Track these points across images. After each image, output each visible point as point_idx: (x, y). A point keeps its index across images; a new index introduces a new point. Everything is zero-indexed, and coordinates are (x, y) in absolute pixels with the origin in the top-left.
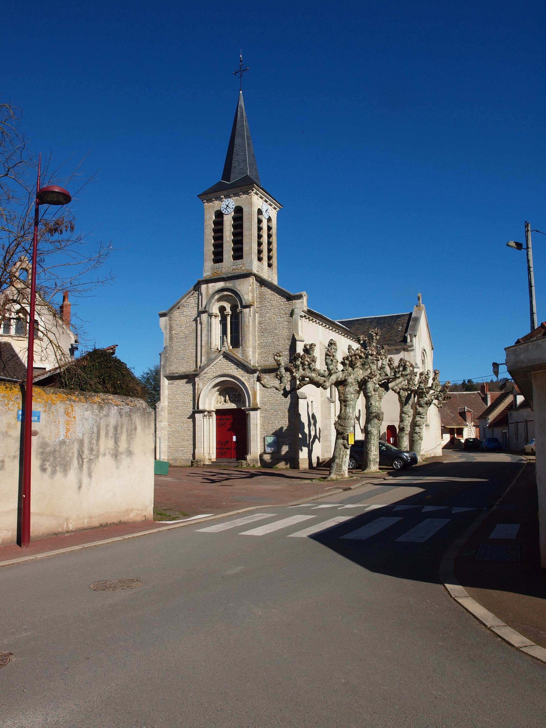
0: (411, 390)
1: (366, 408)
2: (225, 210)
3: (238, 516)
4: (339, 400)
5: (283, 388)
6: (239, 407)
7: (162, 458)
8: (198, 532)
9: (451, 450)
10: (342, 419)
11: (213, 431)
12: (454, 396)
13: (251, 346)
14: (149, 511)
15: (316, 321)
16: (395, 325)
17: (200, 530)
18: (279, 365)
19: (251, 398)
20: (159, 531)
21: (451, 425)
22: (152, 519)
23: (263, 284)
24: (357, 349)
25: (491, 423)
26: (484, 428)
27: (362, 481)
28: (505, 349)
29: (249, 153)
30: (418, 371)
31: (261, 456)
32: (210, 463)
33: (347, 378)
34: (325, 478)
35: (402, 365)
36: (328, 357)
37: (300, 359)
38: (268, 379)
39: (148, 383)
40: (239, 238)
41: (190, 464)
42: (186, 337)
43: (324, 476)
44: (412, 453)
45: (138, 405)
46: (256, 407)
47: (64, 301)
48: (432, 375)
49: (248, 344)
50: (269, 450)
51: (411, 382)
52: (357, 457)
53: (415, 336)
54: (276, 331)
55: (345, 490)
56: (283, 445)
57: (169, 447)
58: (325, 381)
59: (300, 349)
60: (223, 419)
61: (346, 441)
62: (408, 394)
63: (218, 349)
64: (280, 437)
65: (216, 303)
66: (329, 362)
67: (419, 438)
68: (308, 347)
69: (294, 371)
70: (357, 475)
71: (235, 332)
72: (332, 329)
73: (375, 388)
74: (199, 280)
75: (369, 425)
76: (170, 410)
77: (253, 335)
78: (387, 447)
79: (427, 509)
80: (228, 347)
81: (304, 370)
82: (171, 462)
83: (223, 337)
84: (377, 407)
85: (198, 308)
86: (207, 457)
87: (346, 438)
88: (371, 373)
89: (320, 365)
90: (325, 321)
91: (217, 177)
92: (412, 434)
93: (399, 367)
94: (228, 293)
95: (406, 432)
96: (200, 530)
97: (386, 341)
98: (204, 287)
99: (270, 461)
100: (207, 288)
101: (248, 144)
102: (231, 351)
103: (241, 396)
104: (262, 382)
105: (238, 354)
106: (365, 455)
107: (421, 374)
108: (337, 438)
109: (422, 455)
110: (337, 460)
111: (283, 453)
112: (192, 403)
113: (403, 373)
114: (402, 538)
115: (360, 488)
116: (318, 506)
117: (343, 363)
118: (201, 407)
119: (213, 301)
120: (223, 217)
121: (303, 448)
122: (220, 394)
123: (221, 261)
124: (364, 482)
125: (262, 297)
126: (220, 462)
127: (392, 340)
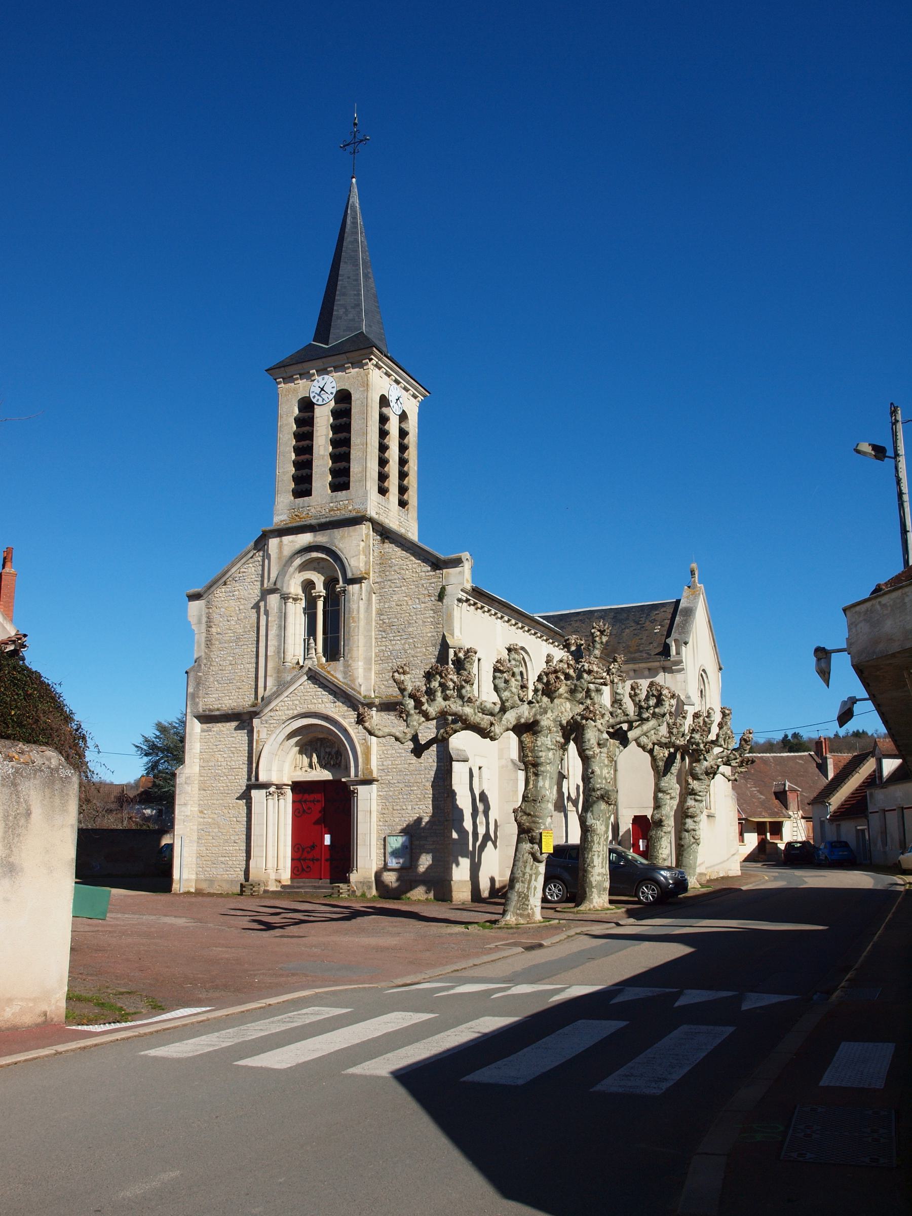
0: (674, 745)
2: (317, 397)
3: (268, 1012)
5: (409, 736)
6: (337, 778)
7: (185, 876)
8: (146, 1056)
9: (759, 865)
11: (285, 824)
12: (764, 761)
13: (361, 657)
14: (56, 1003)
15: (489, 611)
16: (648, 623)
17: (153, 1052)
19: (360, 760)
20: (58, 1053)
21: (760, 815)
22: (63, 1019)
23: (387, 538)
24: (561, 661)
25: (835, 812)
27: (570, 928)
28: (845, 610)
29: (366, 291)
31: (378, 875)
32: (279, 889)
33: (538, 717)
34: (494, 922)
35: (653, 695)
36: (498, 674)
38: (376, 718)
41: (237, 889)
45: (39, 761)
46: (369, 777)
47: (3, 568)
48: (717, 718)
50: (393, 863)
51: (675, 731)
52: (566, 876)
53: (686, 643)
54: (410, 629)
55: (530, 948)
57: (200, 856)
58: (492, 724)
60: (305, 801)
61: (536, 847)
62: (670, 754)
63: (298, 663)
65: (297, 575)
66: (502, 685)
67: (693, 840)
68: (461, 655)
69: (424, 700)
71: (332, 634)
73: (599, 740)
74: (264, 529)
75: (589, 814)
76: (204, 782)
77: (365, 637)
79: (691, 997)
81: (446, 698)
82: (204, 886)
84: (606, 778)
85: (262, 584)
89: (486, 694)
90: (508, 611)
91: (306, 337)
93: (647, 698)
95: (665, 829)
96: (153, 1052)
97: (631, 653)
98: (273, 543)
99: (395, 885)
100: (280, 546)
101: (366, 276)
102: (323, 668)
104: (367, 724)
105: (336, 673)
106: (581, 874)
107: (696, 716)
109: (701, 874)
110: (518, 886)
111: (422, 869)
112: (246, 770)
113: (657, 710)
114: (611, 1084)
115: (563, 944)
116: (453, 987)
118: (263, 778)
119: (291, 569)
122: (301, 752)
125: (384, 563)
126: (298, 887)
127: (641, 652)
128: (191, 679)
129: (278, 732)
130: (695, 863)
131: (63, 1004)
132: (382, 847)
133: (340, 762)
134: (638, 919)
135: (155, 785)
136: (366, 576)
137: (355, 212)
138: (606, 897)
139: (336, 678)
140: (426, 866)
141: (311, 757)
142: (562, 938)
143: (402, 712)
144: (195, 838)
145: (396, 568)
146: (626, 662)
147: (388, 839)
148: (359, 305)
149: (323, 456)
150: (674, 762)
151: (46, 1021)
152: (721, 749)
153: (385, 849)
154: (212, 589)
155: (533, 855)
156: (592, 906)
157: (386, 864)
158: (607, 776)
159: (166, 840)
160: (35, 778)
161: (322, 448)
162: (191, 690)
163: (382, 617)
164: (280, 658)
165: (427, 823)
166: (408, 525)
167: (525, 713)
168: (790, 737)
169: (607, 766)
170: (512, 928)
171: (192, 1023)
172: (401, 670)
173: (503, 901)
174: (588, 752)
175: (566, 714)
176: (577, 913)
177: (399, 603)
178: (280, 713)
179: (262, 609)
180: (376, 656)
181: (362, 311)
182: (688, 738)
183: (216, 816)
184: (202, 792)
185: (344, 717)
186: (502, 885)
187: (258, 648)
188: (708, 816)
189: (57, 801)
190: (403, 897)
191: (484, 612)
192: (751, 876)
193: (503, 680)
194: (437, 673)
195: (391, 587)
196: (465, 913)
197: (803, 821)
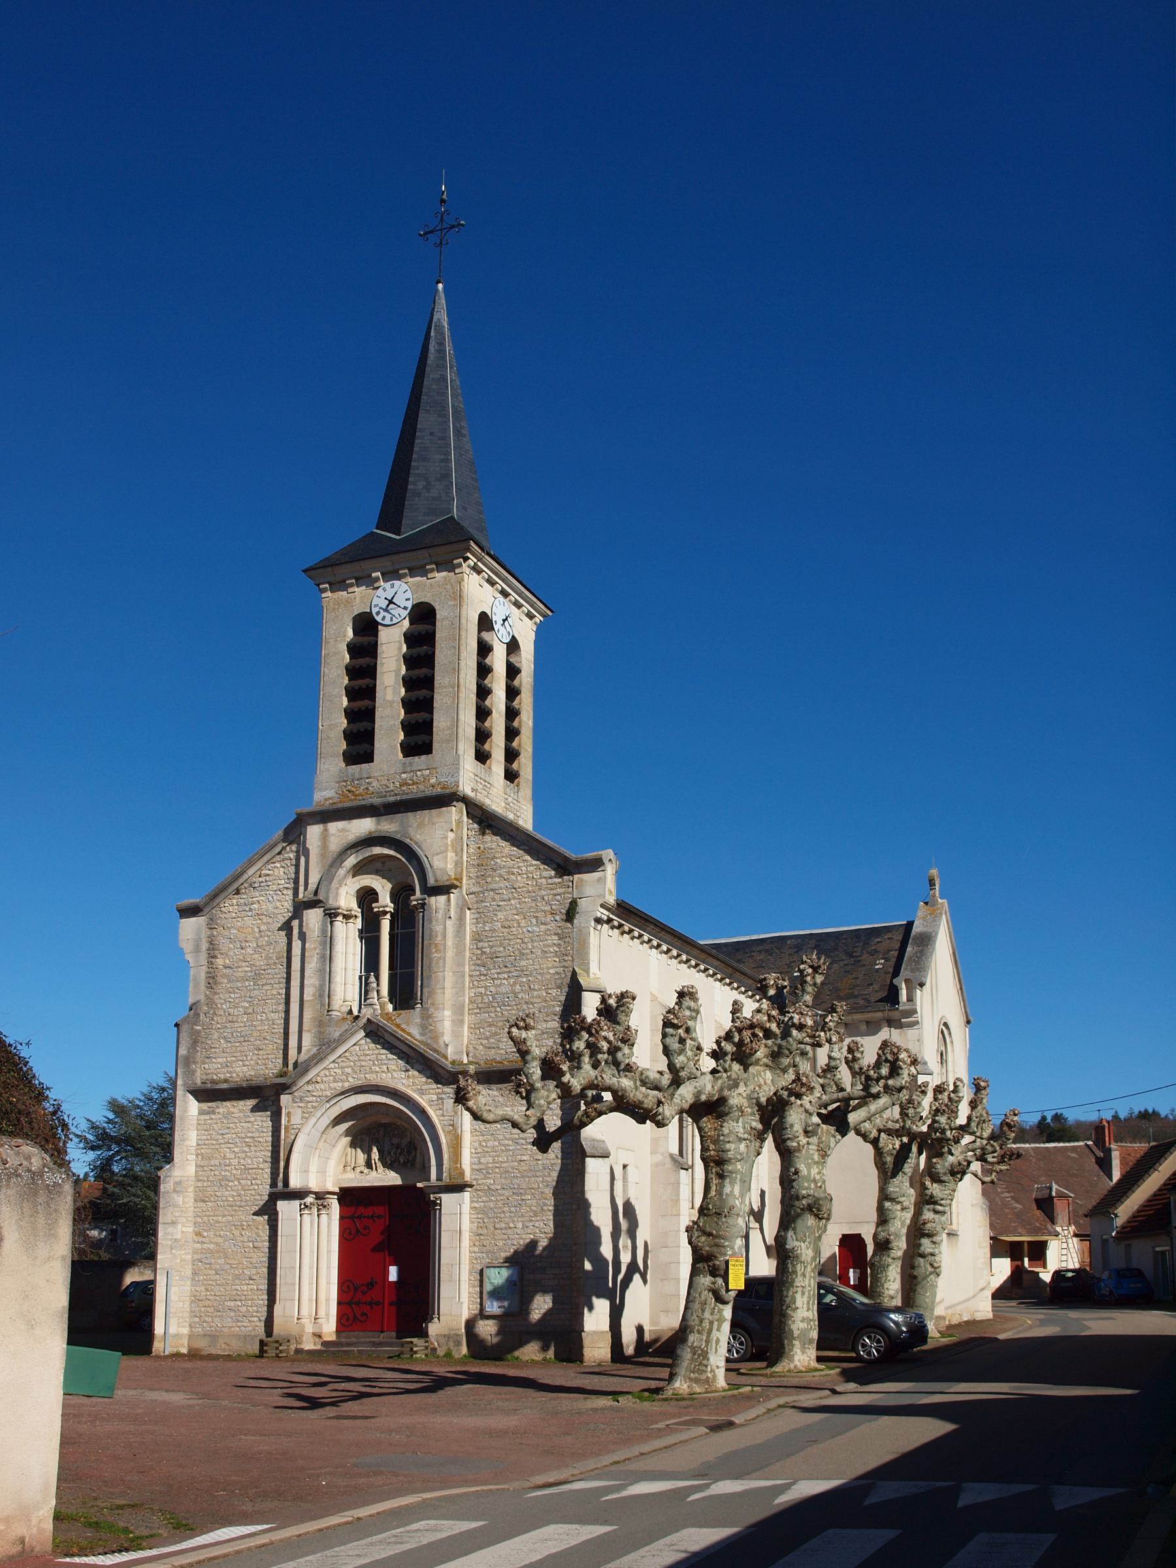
1: (782, 1183)
2: (383, 613)
4: (703, 1159)
6: (410, 1183)
7: (173, 1330)
9: (1014, 1303)
10: (711, 1213)
11: (329, 1252)
15: (640, 936)
16: (865, 956)
18: (524, 1053)
19: (446, 1156)
21: (1014, 1232)
23: (490, 827)
25: (1123, 1227)
26: (1105, 1243)
30: (934, 1081)
31: (470, 1324)
32: (319, 1347)
33: (726, 1093)
34: (657, 1391)
35: (887, 1061)
36: (670, 1030)
37: (585, 1035)
38: (485, 1097)
39: (161, 1115)
40: (423, 693)
41: (255, 1349)
43: (653, 1384)
44: (911, 1313)
45: (13, 1161)
46: (460, 1181)
48: (966, 1094)
49: (439, 998)
50: (493, 1307)
51: (911, 1111)
53: (922, 985)
54: (523, 963)
55: (716, 1428)
57: (196, 1300)
58: (659, 1103)
59: (590, 1006)
60: (359, 1218)
61: (720, 1281)
62: (903, 1145)
63: (350, 1012)
66: (674, 1045)
67: (930, 1269)
68: (612, 1002)
69: (565, 1067)
70: (754, 1380)
72: (688, 961)
73: (807, 1125)
74: (299, 810)
75: (790, 1233)
78: (840, 1295)
79: (973, 1494)
80: (382, 1006)
81: (595, 1066)
82: (202, 1344)
83: (367, 978)
84: (815, 1181)
85: (296, 893)
88: (798, 1079)
89: (646, 1054)
90: (668, 937)
92: (912, 1257)
93: (878, 1065)
94: (386, 851)
98: (313, 832)
99: (495, 1340)
100: (325, 837)
101: (458, 432)
103: (416, 1149)
104: (471, 1104)
105: (410, 1026)
106: (776, 1319)
107: (939, 1090)
108: (694, 1273)
109: (939, 1318)
110: (693, 1338)
111: (536, 1315)
112: (268, 1171)
113: (890, 1082)
115: (762, 1423)
117: (716, 1055)
118: (295, 1182)
119: (342, 872)
120: (375, 634)
121: (594, 1299)
122: (353, 1145)
124: (772, 1404)
125: (484, 865)
126: (348, 1345)
127: (856, 997)
128: (184, 1036)
129: (318, 1114)
130: (933, 1302)
131: (49, 1525)
132: (477, 1283)
134: (861, 1384)
136: (456, 882)
137: (443, 334)
138: (812, 1353)
139: (409, 1034)
140: (543, 1311)
141: (368, 1153)
142: (760, 1413)
143: (519, 1086)
144: (189, 1272)
145: (503, 872)
146: (849, 1013)
147: (487, 1272)
148: (449, 475)
149: (392, 702)
150: (908, 1157)
151: (23, 1551)
152: (973, 1138)
153: (481, 1286)
154: (217, 901)
156: (792, 1366)
157: (482, 1309)
158: (818, 1177)
159: (132, 1276)
160: (8, 1186)
161: (389, 692)
162: (183, 1051)
163: (480, 945)
164: (322, 1005)
165: (545, 1249)
167: (708, 1087)
168: (1049, 1120)
169: (817, 1163)
170: (684, 1399)
171: (249, 1549)
172: (522, 1024)
173: (670, 1361)
174: (789, 1143)
175: (766, 1088)
176: (772, 1375)
177: (507, 924)
178: (322, 1086)
179: (296, 931)
180: (471, 1002)
181: (451, 480)
182: (929, 1122)
183: (220, 1240)
184: (200, 1204)
185: (422, 1092)
186: (654, 1337)
187: (288, 989)
188: (949, 1234)
189: (41, 1220)
190: (509, 1356)
191: (633, 938)
192: (1007, 1320)
193: (677, 1039)
194: (583, 1029)
195: (494, 900)
196: (605, 1379)
197: (1075, 1239)
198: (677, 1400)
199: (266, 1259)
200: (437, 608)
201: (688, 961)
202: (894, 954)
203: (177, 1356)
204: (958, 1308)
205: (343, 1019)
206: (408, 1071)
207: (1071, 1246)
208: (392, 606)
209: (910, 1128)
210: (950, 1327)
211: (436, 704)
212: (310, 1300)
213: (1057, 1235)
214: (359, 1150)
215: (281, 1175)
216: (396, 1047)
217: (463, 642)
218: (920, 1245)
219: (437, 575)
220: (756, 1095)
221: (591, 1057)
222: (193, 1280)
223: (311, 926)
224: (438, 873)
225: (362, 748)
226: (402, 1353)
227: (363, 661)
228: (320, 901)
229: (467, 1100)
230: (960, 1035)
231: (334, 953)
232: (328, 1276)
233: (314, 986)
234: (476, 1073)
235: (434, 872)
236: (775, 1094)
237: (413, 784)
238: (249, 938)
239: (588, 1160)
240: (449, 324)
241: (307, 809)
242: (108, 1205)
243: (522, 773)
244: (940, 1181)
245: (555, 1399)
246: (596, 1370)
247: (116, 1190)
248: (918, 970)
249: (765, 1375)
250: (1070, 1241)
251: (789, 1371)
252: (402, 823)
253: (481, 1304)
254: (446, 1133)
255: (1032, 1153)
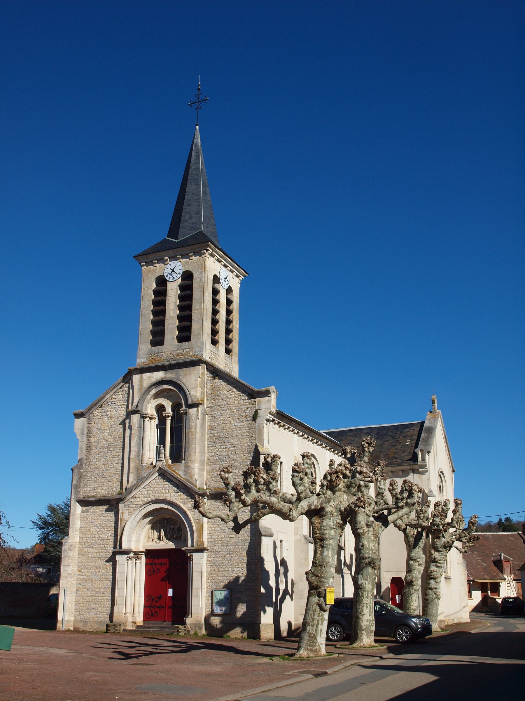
0: (421, 526)
2: (169, 276)
5: (231, 518)
6: (179, 547)
7: (66, 618)
9: (483, 614)
10: (318, 564)
12: (486, 538)
15: (289, 428)
16: (401, 438)
18: (227, 485)
19: (195, 535)
21: (483, 578)
23: (217, 375)
24: (340, 465)
27: (346, 660)
29: (205, 203)
32: (134, 628)
33: (324, 505)
34: (292, 655)
35: (406, 490)
36: (295, 474)
38: (207, 504)
41: (104, 628)
42: (109, 446)
46: (201, 547)
48: (452, 506)
49: (193, 458)
50: (218, 610)
51: (421, 515)
53: (429, 452)
54: (232, 441)
55: (317, 675)
56: (238, 603)
57: (77, 603)
58: (291, 510)
60: (155, 564)
61: (322, 599)
62: (418, 532)
63: (152, 464)
64: (235, 591)
66: (298, 481)
67: (435, 596)
68: (269, 460)
69: (242, 492)
70: (343, 651)
73: (368, 522)
74: (130, 368)
75: (360, 576)
81: (258, 491)
82: (80, 625)
83: (160, 448)
84: (372, 550)
85: (128, 407)
86: (130, 619)
87: (323, 595)
89: (286, 487)
91: (161, 233)
93: (402, 492)
95: (415, 587)
97: (389, 459)
98: (136, 378)
99: (219, 626)
100: (141, 380)
101: (205, 193)
103: (181, 531)
104: (201, 509)
106: (354, 620)
107: (437, 505)
108: (310, 595)
109: (441, 621)
110: (309, 629)
111: (239, 615)
112: (113, 540)
113: (409, 501)
115: (342, 672)
118: (125, 546)
119: (149, 397)
120: (166, 285)
122: (152, 528)
123: (162, 343)
125: (214, 394)
126: (148, 627)
127: (397, 458)
128: (75, 474)
129: (136, 513)
130: (437, 613)
132: (210, 598)
133: (181, 536)
134: (396, 654)
135: (45, 550)
136: (201, 402)
137: (198, 149)
138: (372, 638)
141: (159, 532)
142: (341, 668)
143: (226, 500)
144: (75, 590)
145: (223, 397)
147: (214, 592)
150: (421, 539)
153: (212, 600)
154: (92, 410)
155: (320, 606)
156: (362, 644)
157: (212, 611)
158: (373, 548)
159: (53, 591)
161: (172, 312)
162: (75, 482)
163: (212, 432)
164: (139, 460)
165: (243, 581)
166: (233, 368)
167: (315, 502)
168: (503, 521)
169: (373, 541)
170: (304, 660)
172: (226, 470)
173: (297, 639)
175: (344, 503)
178: (138, 500)
179: (127, 425)
180: (208, 459)
181: (202, 214)
182: (431, 521)
183: (90, 574)
184: (81, 556)
185: (184, 503)
186: (296, 627)
187: (123, 452)
188: (446, 578)
191: (285, 429)
193: (299, 478)
194: (252, 473)
195: (219, 410)
196: (270, 648)
197: (514, 582)
198: (301, 660)
199: (111, 584)
200: (194, 273)
201: (312, 440)
202: (415, 437)
203: (68, 631)
204: (452, 617)
205: (148, 467)
206: (178, 492)
207: (512, 585)
208: (173, 272)
209: (421, 524)
210: (448, 626)
211: (193, 318)
212: (131, 605)
213: (505, 579)
214: (155, 531)
215: (118, 543)
216: (173, 481)
217: (205, 289)
218: (429, 583)
219: (194, 258)
220: (339, 507)
221: (255, 487)
222: (77, 593)
223: (134, 422)
224: (193, 397)
225: (159, 338)
226: (173, 632)
227: (160, 298)
228: (139, 411)
229: (199, 507)
230: (449, 477)
231: (144, 436)
232: (140, 593)
233: (135, 451)
234: (210, 494)
235: (191, 398)
236: (348, 506)
237: (182, 355)
238: (106, 428)
239: (263, 538)
240: (201, 143)
241: (133, 368)
242: (46, 556)
243: (233, 350)
244: (439, 551)
245: (242, 658)
246: (266, 643)
247: (50, 549)
248: (427, 445)
249: (349, 649)
250: (511, 583)
251: (360, 647)
252: (177, 374)
253: (212, 608)
254: (196, 523)
255: (491, 537)
